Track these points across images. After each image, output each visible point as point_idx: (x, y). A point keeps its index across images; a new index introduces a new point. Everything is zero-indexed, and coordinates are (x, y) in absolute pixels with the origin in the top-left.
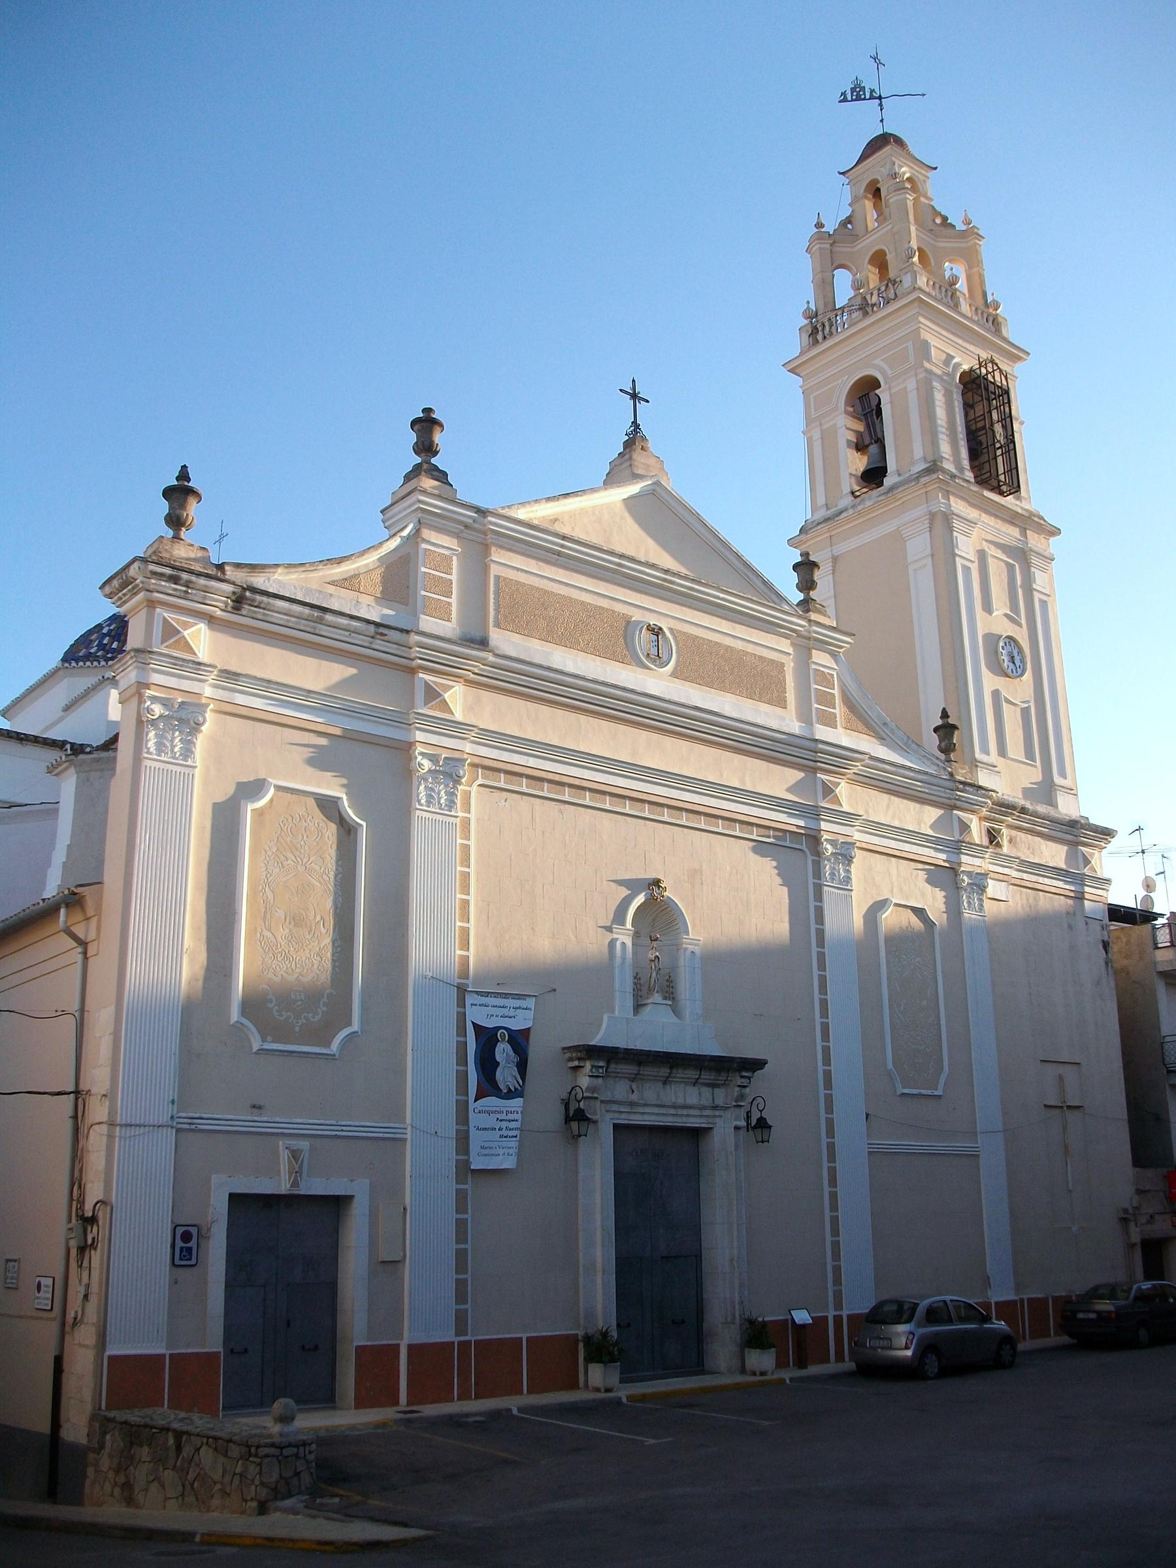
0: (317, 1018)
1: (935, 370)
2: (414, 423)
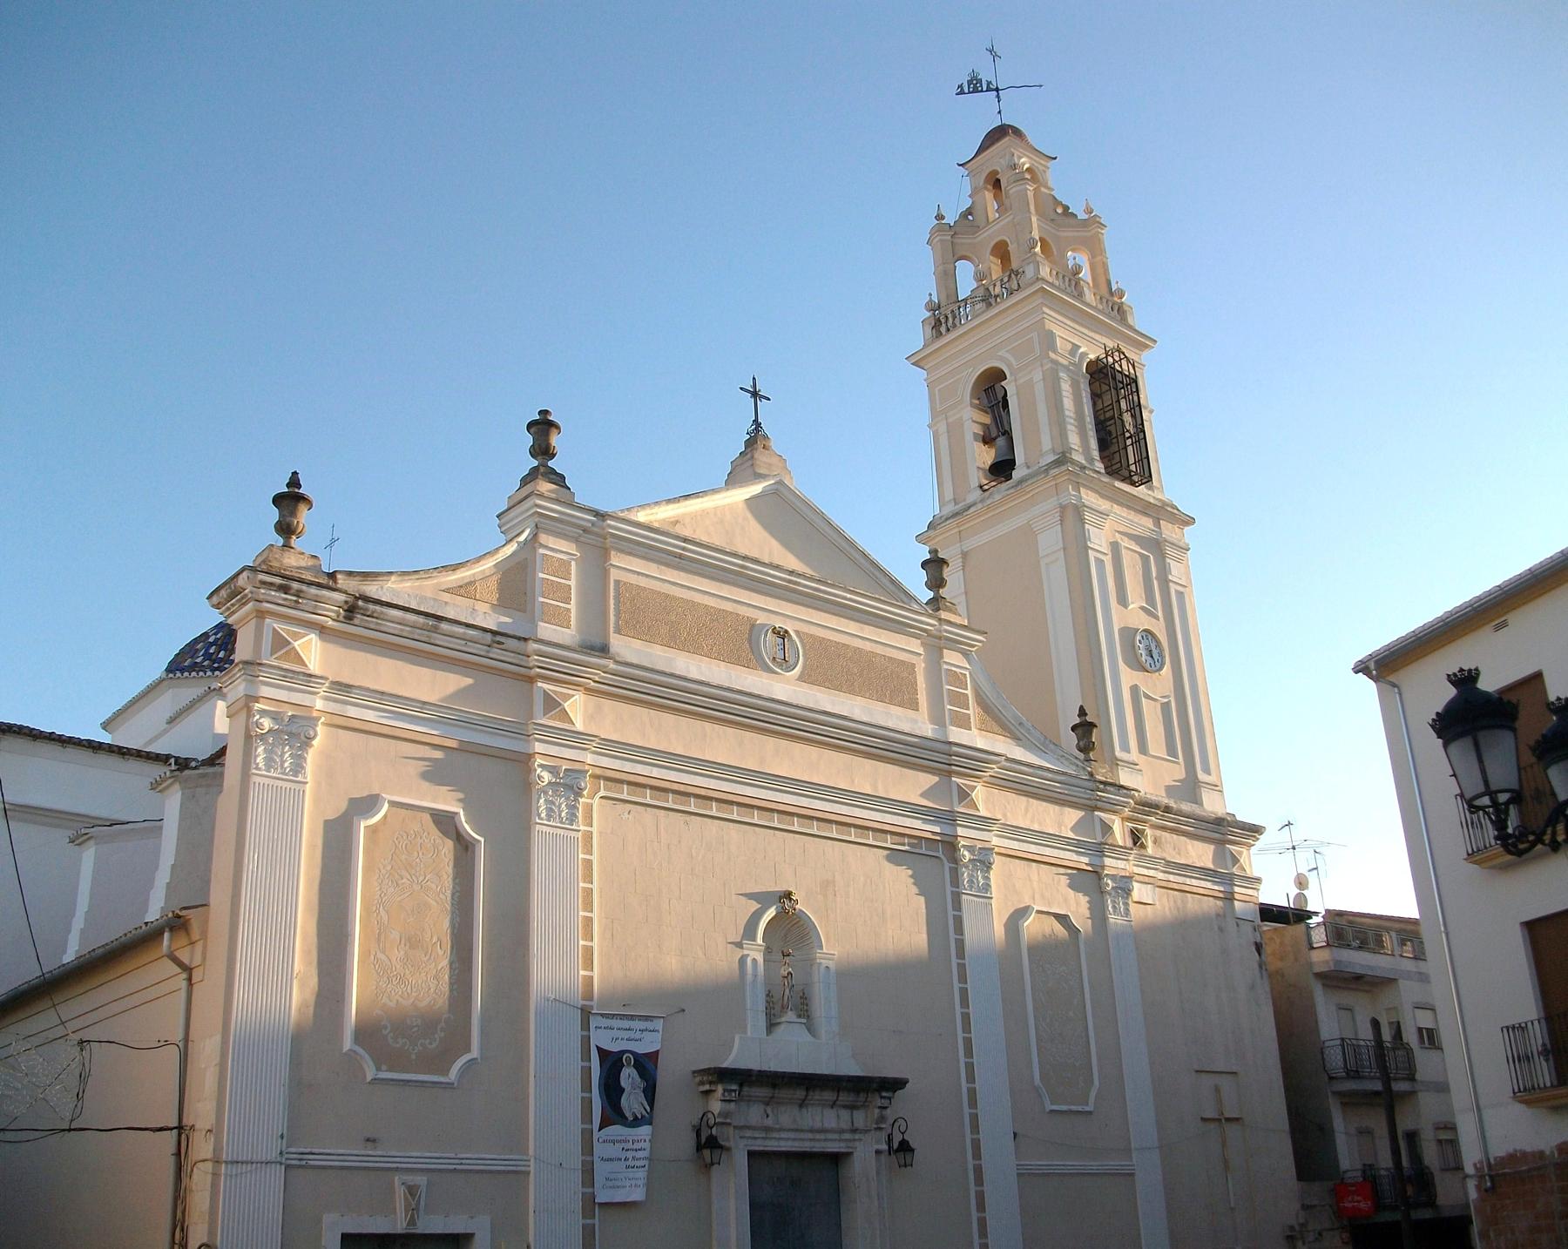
2: (530, 426)
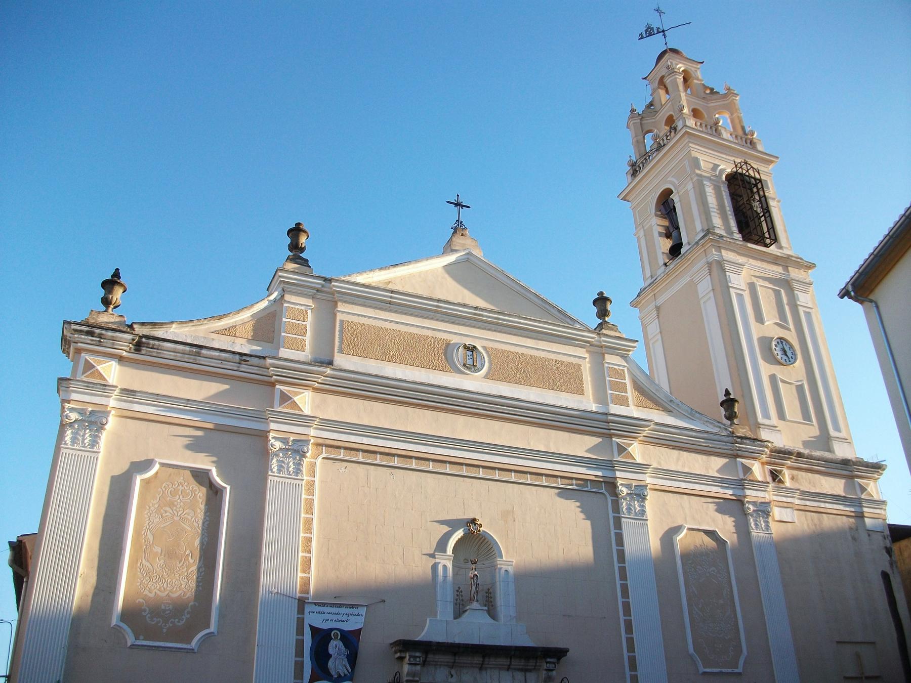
0: (182, 623)
1: (704, 174)
2: (290, 231)
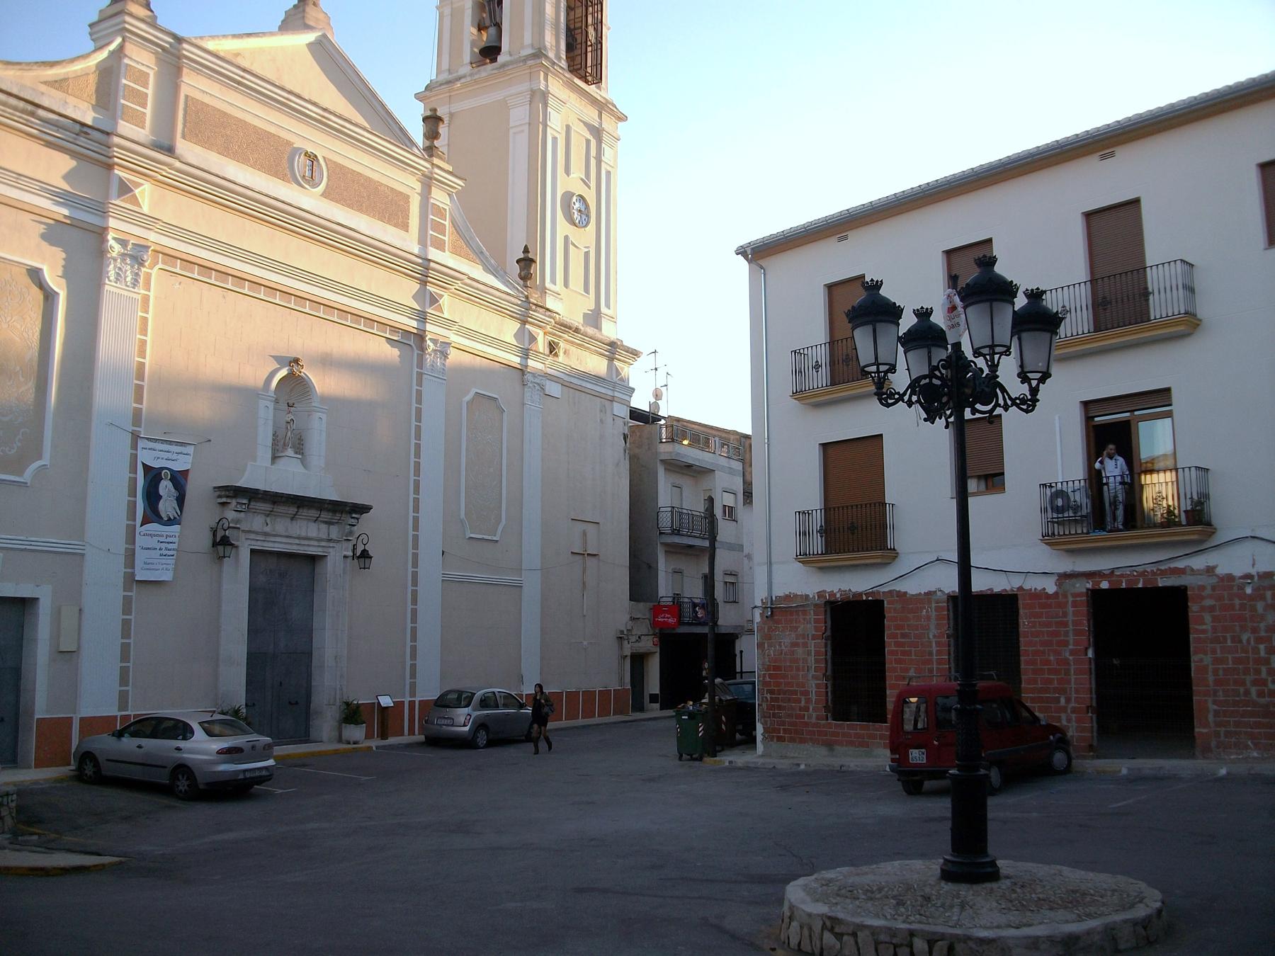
0: (13, 451)
